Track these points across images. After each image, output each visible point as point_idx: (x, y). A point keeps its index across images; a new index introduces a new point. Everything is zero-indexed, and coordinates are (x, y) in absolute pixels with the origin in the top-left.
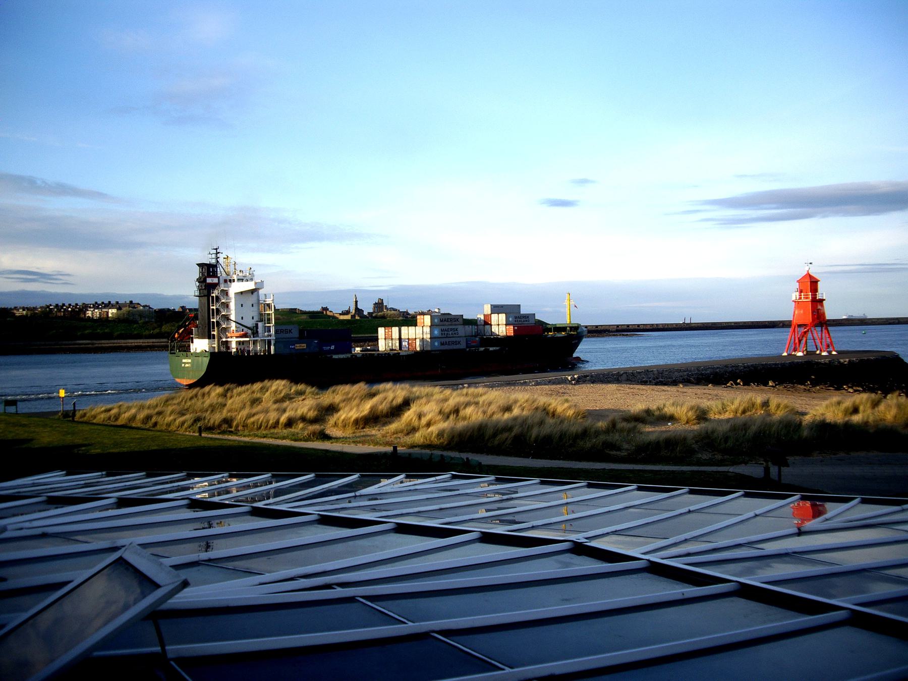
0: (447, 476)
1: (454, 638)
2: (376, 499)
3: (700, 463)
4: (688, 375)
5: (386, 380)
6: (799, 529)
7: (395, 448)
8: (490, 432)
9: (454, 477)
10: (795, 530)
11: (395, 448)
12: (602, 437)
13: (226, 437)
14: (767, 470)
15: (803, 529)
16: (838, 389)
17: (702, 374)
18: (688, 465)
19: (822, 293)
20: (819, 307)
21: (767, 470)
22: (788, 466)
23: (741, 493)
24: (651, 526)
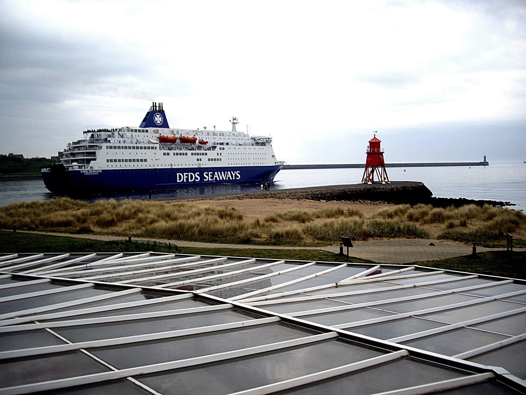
0: (148, 253)
1: (93, 353)
2: (92, 269)
3: (305, 245)
4: (306, 195)
5: (99, 197)
6: (336, 284)
7: (130, 238)
8: (186, 227)
9: (152, 255)
10: (335, 285)
11: (130, 238)
12: (250, 230)
13: (31, 232)
14: (341, 249)
15: (339, 284)
16: (389, 203)
17: (314, 194)
18: (299, 246)
19: (383, 147)
20: (381, 157)
21: (341, 249)
22: (352, 247)
23: (314, 262)
24: (392, 292)
